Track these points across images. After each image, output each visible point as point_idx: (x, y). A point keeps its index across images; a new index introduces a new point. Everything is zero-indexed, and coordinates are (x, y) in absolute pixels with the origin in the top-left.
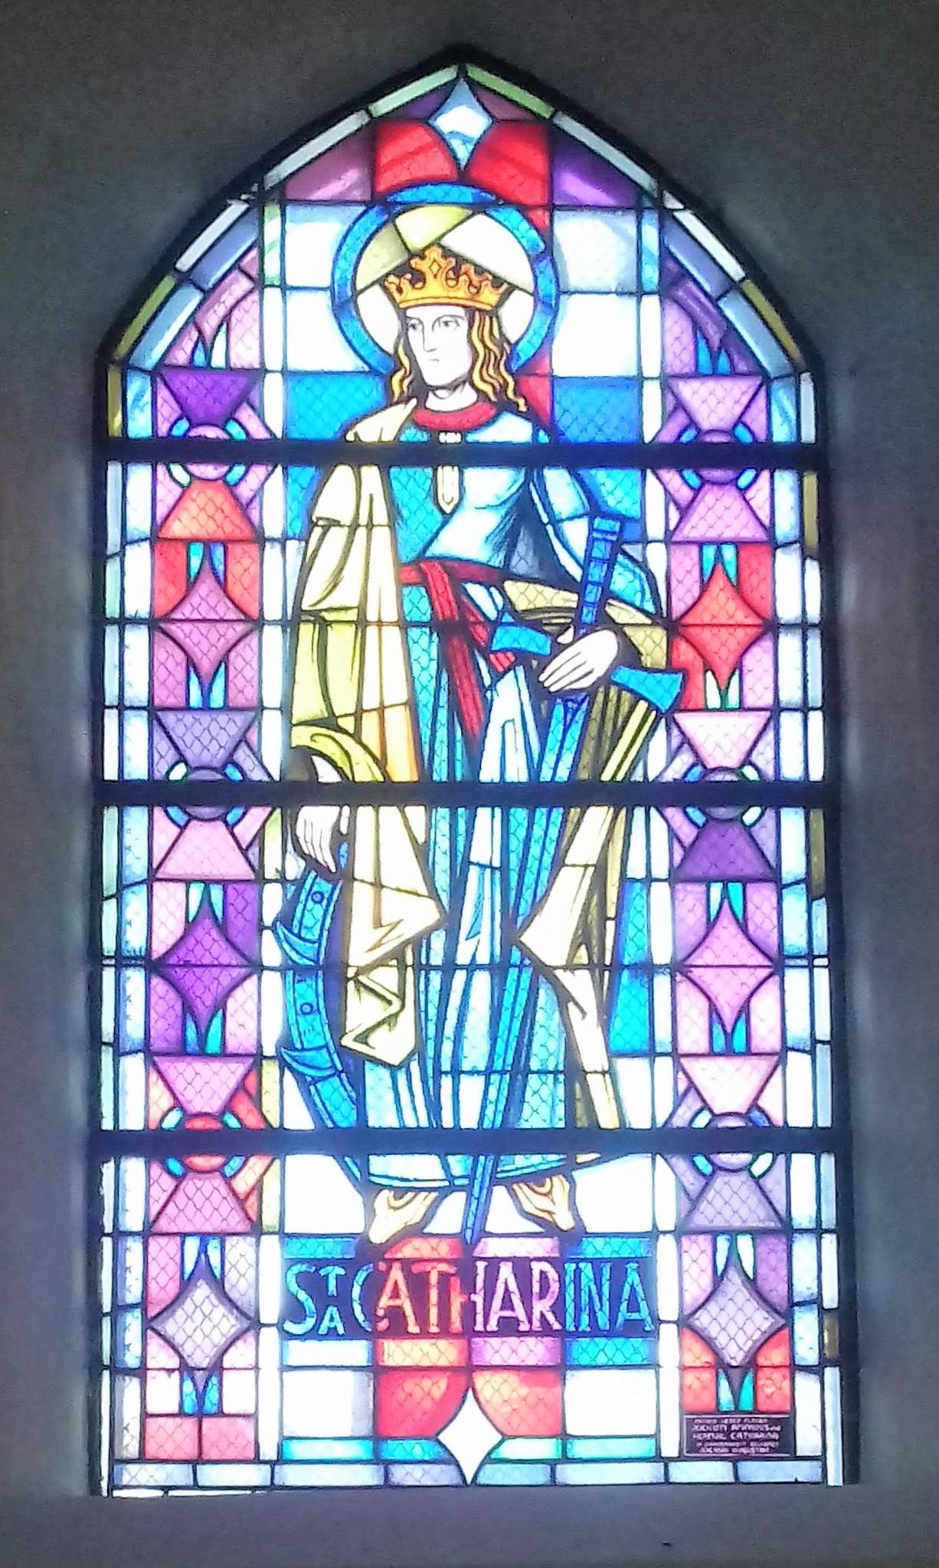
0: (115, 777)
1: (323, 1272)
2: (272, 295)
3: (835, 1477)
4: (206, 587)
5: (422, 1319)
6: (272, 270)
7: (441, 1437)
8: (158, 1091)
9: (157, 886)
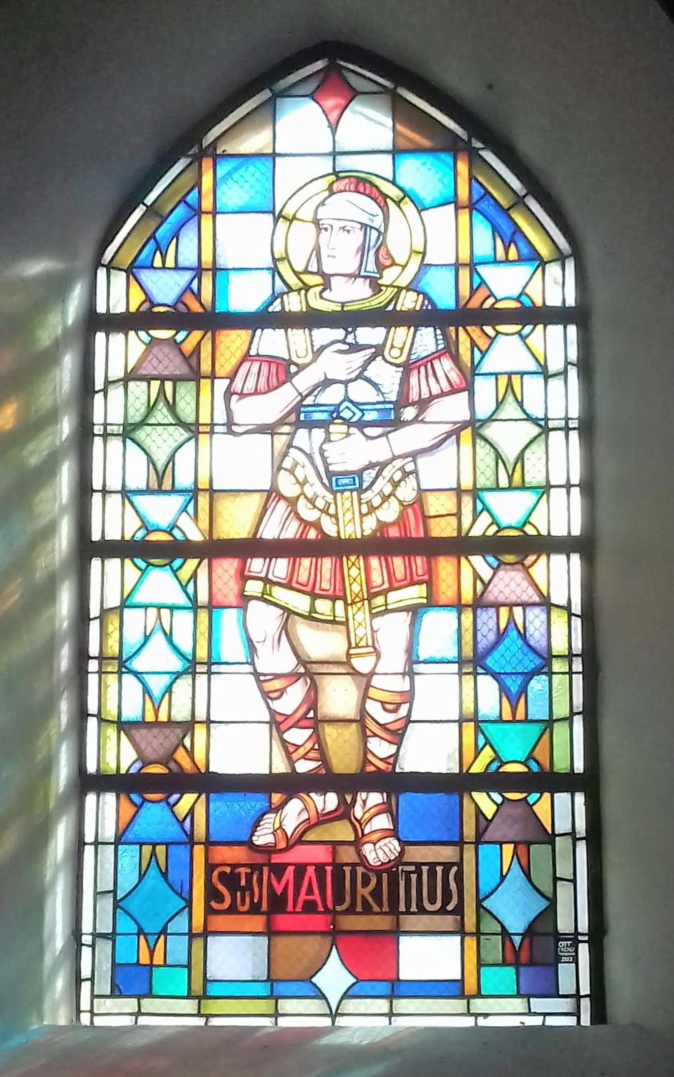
0: (104, 312)
1: (237, 871)
3: (586, 1020)
4: (157, 692)
6: (207, 204)
7: (314, 980)
8: (135, 289)
9: (126, 611)
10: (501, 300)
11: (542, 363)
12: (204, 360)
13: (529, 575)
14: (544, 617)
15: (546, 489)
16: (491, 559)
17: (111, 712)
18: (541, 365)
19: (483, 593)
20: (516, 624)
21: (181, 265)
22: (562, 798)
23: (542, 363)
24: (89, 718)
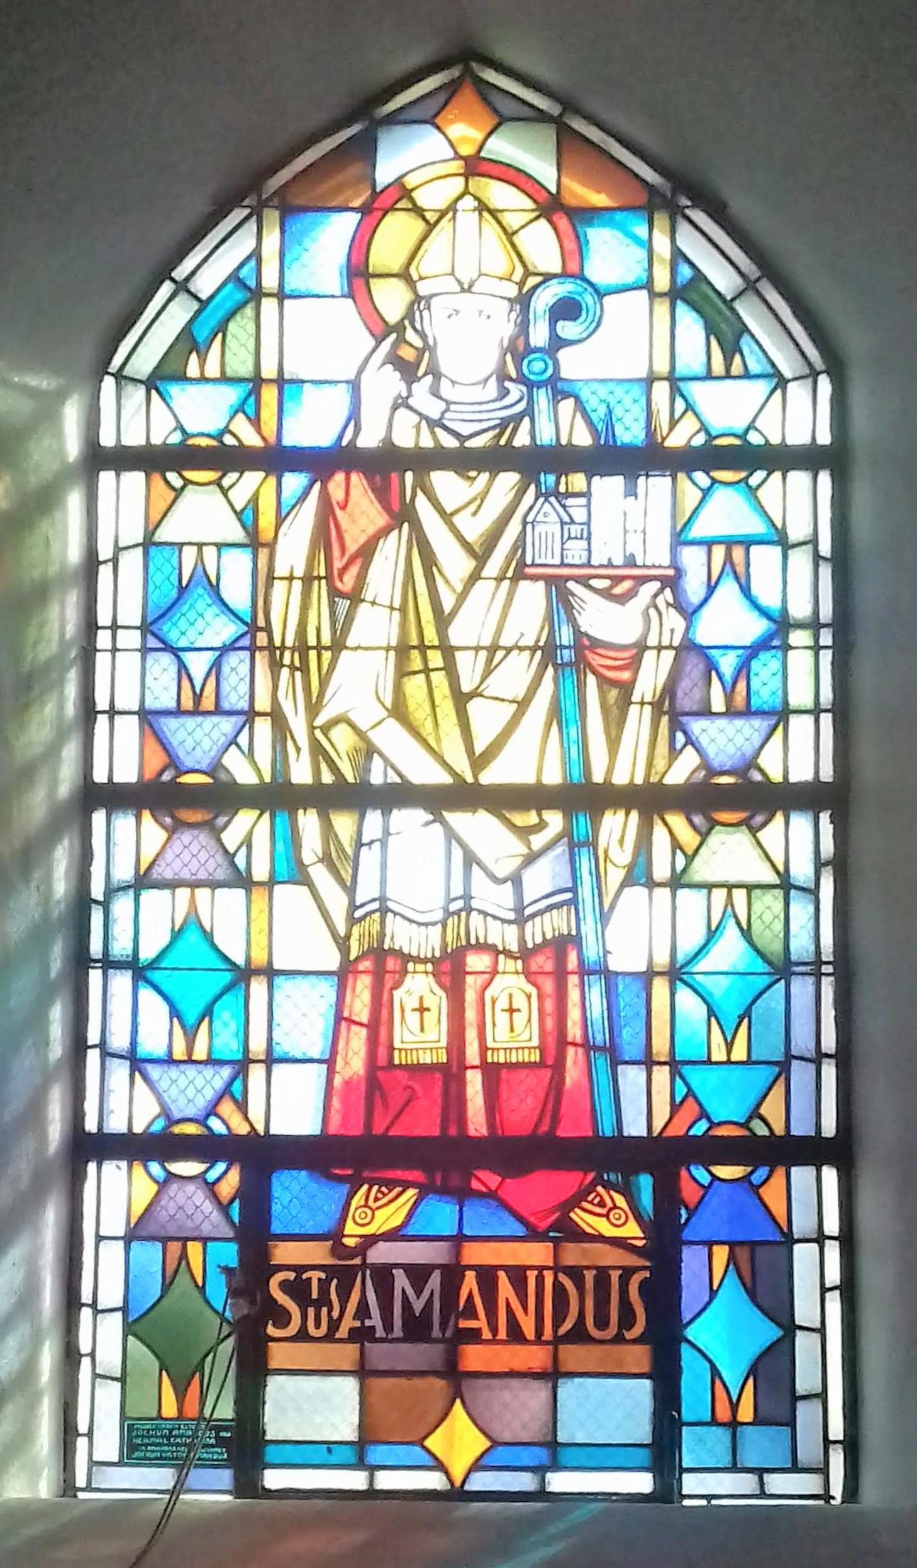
1: (304, 1276)
2: (269, 306)
5: (494, 1330)
10: (720, 1124)
11: (781, 868)
12: (262, 911)
13: (761, 1199)
14: (779, 906)
15: (782, 714)
16: (698, 820)
17: (119, 1041)
18: (778, 872)
19: (684, 870)
20: (736, 917)
21: (229, 373)
22: (802, 1176)
23: (781, 868)
24: (99, 631)
